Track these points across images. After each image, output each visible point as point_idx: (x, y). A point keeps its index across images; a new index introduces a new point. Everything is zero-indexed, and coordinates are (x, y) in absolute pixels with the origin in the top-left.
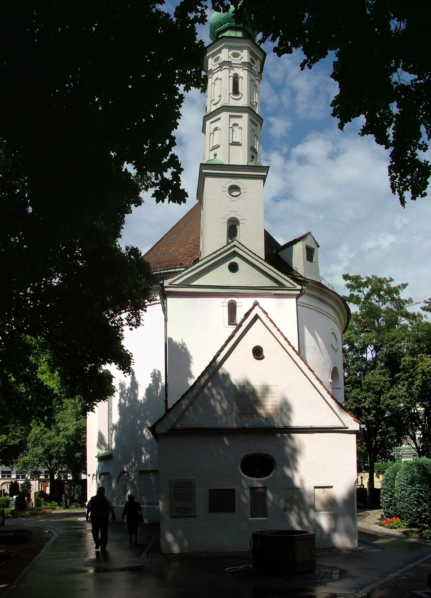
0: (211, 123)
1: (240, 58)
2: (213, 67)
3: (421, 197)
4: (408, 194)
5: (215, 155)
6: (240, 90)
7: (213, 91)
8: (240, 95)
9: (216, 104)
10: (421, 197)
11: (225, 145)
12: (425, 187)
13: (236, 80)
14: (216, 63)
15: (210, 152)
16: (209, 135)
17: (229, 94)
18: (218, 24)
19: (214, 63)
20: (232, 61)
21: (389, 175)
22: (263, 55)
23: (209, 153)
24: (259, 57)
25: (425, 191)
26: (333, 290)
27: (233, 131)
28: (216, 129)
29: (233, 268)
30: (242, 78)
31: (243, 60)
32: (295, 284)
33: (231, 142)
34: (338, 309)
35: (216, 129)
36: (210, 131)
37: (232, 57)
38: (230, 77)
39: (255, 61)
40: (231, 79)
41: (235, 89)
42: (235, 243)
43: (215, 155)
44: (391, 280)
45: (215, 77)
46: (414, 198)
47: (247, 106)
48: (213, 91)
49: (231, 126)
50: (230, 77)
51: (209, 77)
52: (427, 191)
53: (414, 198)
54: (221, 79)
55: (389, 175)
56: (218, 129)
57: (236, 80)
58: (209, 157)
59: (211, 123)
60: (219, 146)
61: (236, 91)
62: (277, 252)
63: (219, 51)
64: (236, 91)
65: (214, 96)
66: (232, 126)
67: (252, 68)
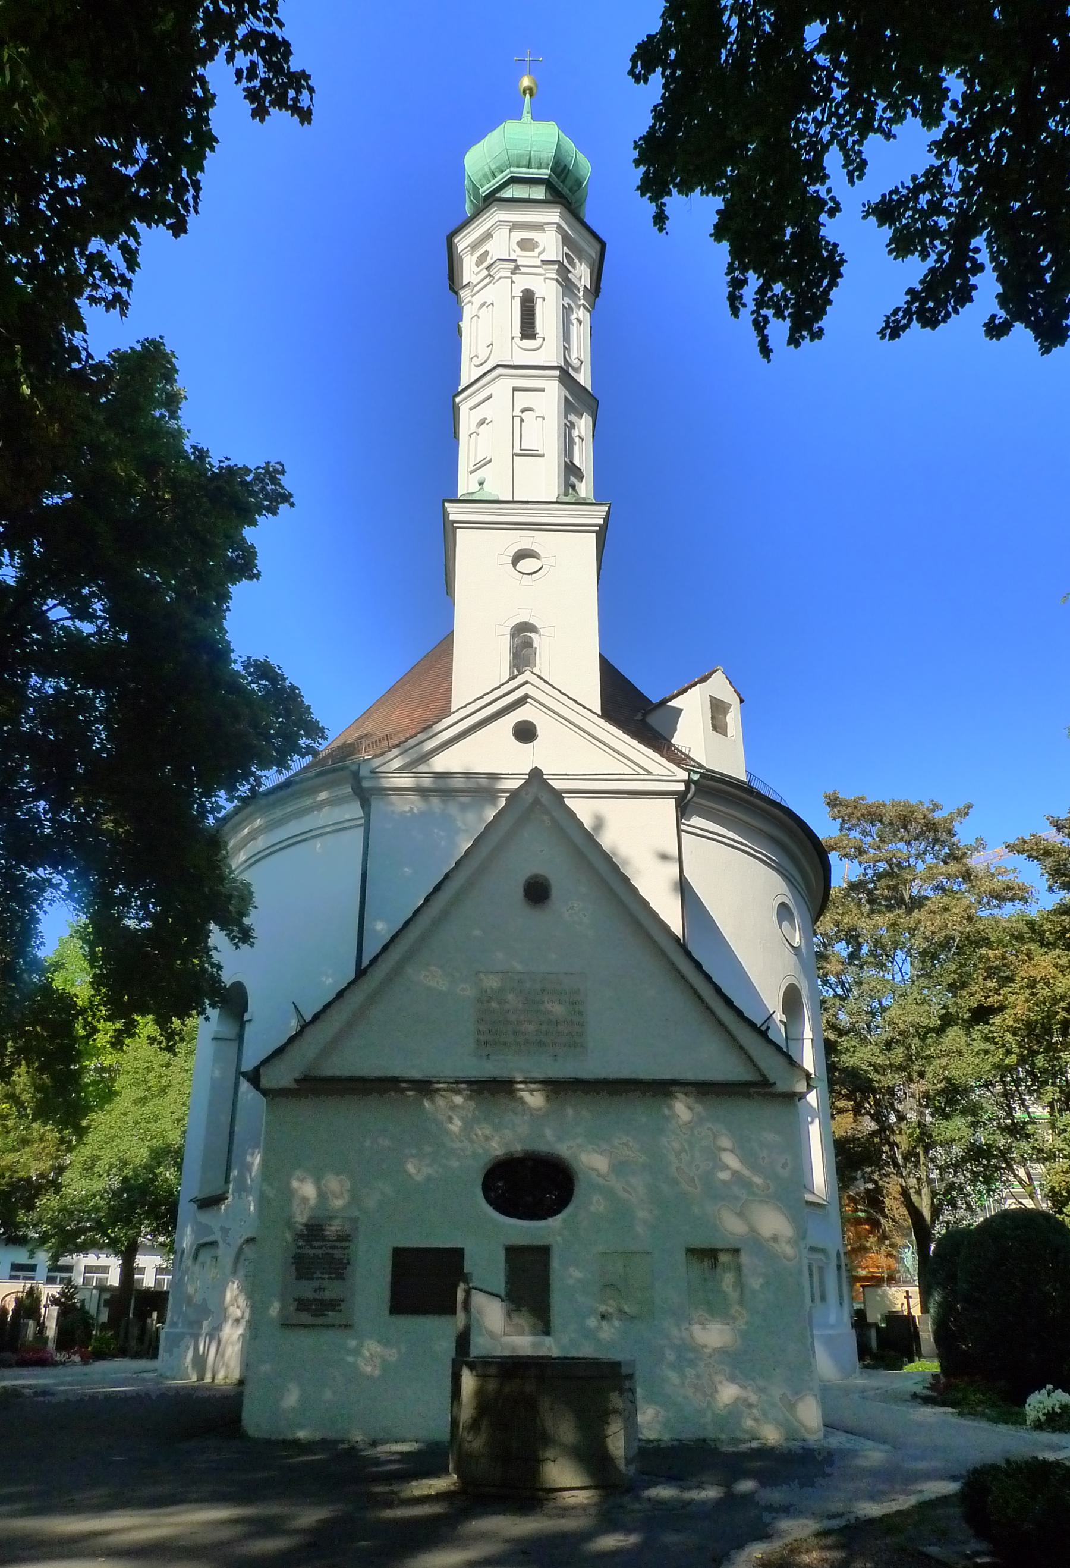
0: (471, 409)
1: (537, 251)
2: (474, 276)
3: (812, 340)
4: (779, 329)
5: (481, 484)
6: (539, 328)
7: (474, 334)
8: (539, 341)
9: (482, 364)
10: (812, 340)
11: (502, 456)
12: (820, 313)
13: (528, 303)
14: (481, 267)
15: (471, 476)
16: (467, 436)
17: (513, 338)
18: (485, 175)
19: (477, 270)
20: (518, 259)
21: (727, 274)
22: (598, 247)
23: (468, 480)
24: (586, 252)
25: (820, 324)
26: (783, 803)
27: (522, 421)
28: (482, 422)
29: (525, 733)
30: (544, 300)
31: (544, 257)
32: (673, 767)
33: (517, 450)
34: (794, 847)
35: (482, 422)
36: (469, 429)
37: (518, 249)
38: (513, 297)
39: (576, 261)
40: (517, 303)
41: (526, 323)
42: (527, 676)
43: (481, 484)
44: (936, 807)
45: (477, 300)
46: (794, 341)
47: (555, 364)
48: (474, 334)
49: (517, 412)
50: (513, 297)
51: (466, 301)
52: (824, 323)
53: (794, 341)
54: (492, 304)
55: (727, 274)
56: (487, 422)
57: (528, 303)
58: (468, 487)
59: (471, 409)
60: (490, 461)
61: (528, 329)
62: (644, 715)
63: (488, 236)
64: (528, 329)
65: (476, 348)
66: (520, 414)
67: (570, 275)
